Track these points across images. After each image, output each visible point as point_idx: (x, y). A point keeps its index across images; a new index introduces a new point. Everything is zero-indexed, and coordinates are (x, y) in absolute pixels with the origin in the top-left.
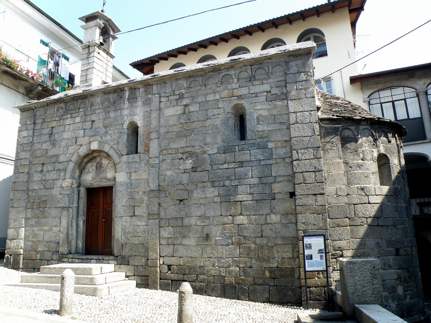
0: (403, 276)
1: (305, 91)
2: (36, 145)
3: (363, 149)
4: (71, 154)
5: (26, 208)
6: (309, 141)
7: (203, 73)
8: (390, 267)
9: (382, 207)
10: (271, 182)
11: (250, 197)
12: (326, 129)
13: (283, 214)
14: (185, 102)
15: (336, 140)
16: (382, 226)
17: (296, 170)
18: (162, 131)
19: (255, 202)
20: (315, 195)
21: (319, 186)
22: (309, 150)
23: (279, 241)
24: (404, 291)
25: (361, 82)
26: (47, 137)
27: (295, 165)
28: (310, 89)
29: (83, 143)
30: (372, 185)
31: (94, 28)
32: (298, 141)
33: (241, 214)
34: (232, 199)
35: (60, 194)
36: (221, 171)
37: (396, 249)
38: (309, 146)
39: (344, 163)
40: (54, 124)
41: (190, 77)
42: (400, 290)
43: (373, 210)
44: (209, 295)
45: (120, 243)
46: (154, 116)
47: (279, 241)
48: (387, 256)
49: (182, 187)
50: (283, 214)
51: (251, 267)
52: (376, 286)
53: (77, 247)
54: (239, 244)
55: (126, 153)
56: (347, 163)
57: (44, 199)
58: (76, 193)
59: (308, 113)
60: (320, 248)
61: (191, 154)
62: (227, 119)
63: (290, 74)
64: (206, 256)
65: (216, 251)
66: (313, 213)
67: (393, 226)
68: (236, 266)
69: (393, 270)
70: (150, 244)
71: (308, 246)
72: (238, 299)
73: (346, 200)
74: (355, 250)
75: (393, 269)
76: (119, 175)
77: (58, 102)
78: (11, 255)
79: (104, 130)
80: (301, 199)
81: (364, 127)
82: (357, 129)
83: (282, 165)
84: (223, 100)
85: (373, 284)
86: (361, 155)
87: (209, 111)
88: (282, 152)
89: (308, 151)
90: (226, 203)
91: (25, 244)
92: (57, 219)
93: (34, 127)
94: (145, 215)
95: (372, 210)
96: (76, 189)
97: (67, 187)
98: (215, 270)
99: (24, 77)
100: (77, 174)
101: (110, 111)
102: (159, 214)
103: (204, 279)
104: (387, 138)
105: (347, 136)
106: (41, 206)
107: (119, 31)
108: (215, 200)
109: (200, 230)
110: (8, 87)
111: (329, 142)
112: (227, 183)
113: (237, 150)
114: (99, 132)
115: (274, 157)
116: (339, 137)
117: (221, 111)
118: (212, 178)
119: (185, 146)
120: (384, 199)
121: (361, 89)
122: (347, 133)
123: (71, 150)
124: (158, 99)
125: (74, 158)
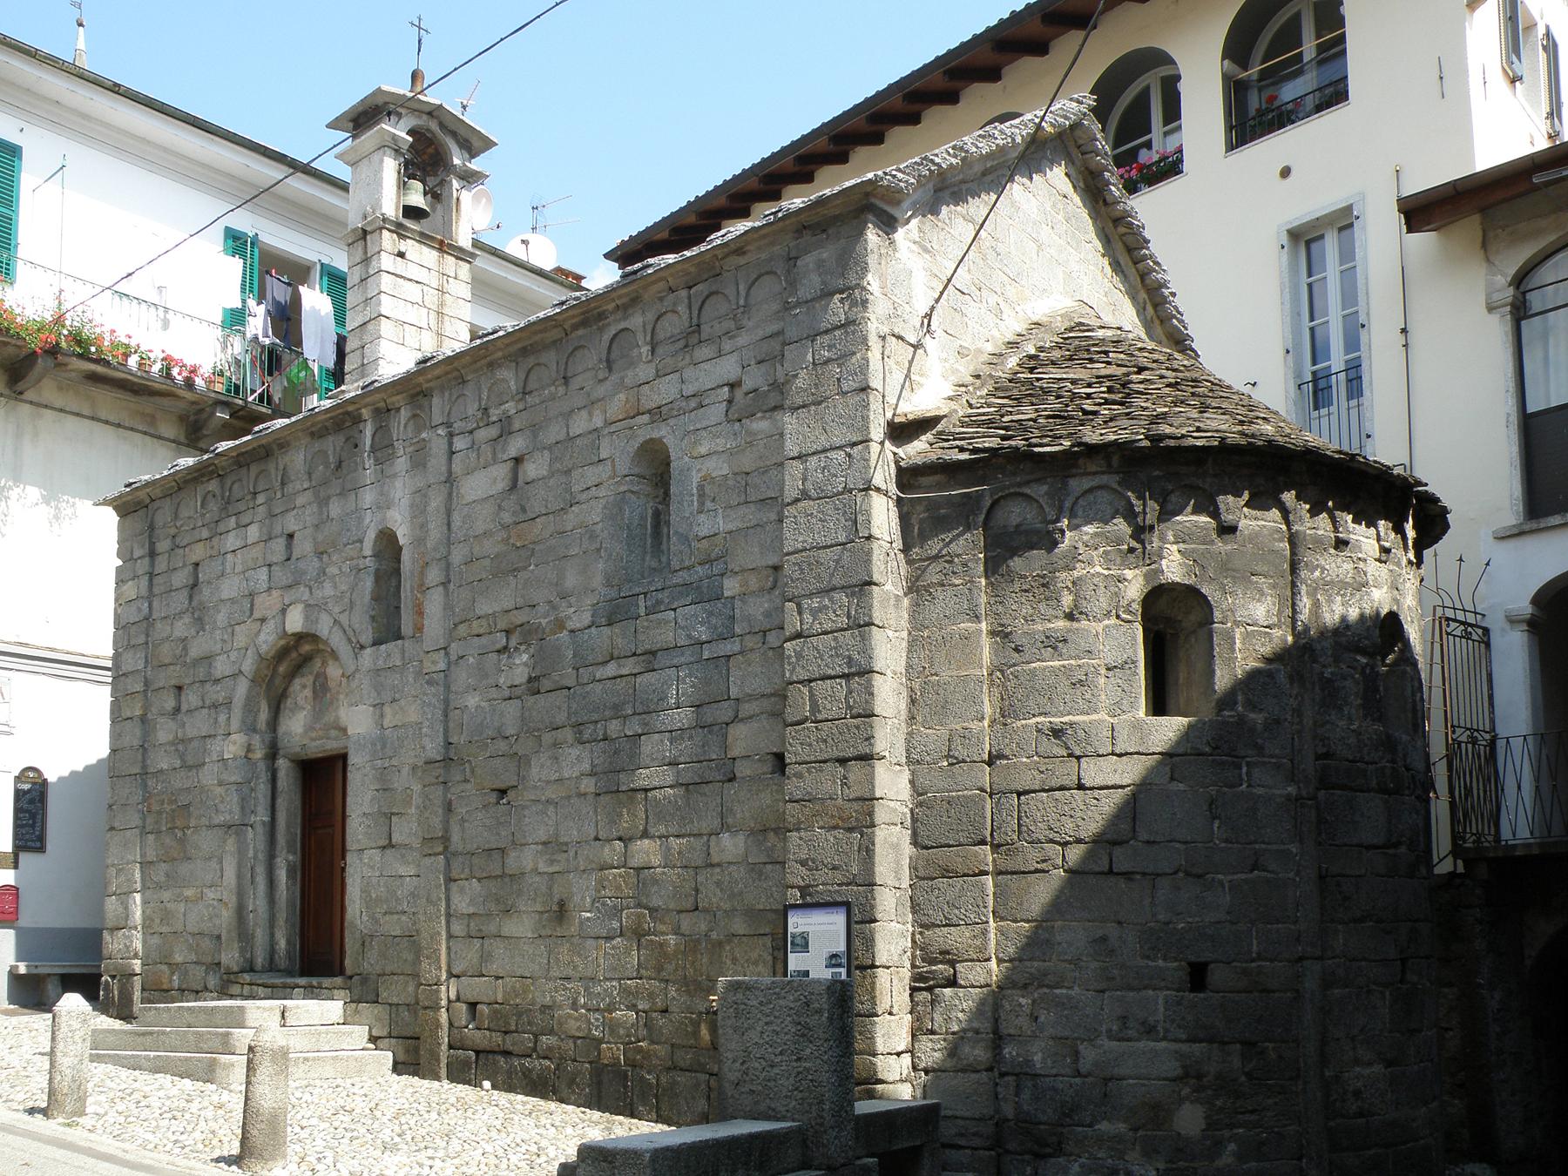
1: (840, 366)
2: (159, 625)
4: (239, 649)
5: (144, 832)
6: (837, 562)
7: (556, 334)
8: (1149, 1031)
10: (726, 719)
11: (669, 776)
12: (932, 505)
13: (752, 832)
14: (516, 446)
15: (968, 546)
16: (1127, 875)
17: (792, 671)
18: (457, 556)
19: (682, 791)
20: (843, 761)
21: (857, 727)
22: (836, 596)
23: (739, 926)
24: (1211, 1125)
25: (1482, 210)
26: (180, 600)
27: (789, 657)
28: (854, 360)
29: (269, 614)
31: (376, 157)
32: (805, 566)
33: (645, 834)
34: (626, 782)
35: (220, 784)
36: (598, 687)
39: (993, 633)
40: (198, 552)
41: (525, 352)
42: (1190, 1120)
44: (562, 1101)
45: (358, 935)
46: (434, 504)
47: (739, 926)
49: (502, 746)
50: (752, 832)
51: (666, 1011)
53: (272, 952)
54: (638, 934)
55: (370, 641)
56: (1007, 635)
57: (183, 800)
58: (264, 777)
59: (840, 456)
60: (834, 950)
61: (521, 633)
62: (621, 500)
63: (798, 304)
64: (557, 974)
65: (580, 955)
66: (835, 827)
67: (1188, 874)
68: (628, 1008)
69: (1164, 1044)
70: (424, 934)
71: (798, 940)
72: (632, 1116)
73: (985, 776)
74: (1010, 961)
75: (1165, 1038)
76: (354, 718)
77: (203, 475)
78: (113, 977)
79: (316, 563)
80: (799, 776)
81: (1087, 483)
83: (755, 657)
84: (613, 428)
85: (799, 1059)
86: (1067, 600)
87: (576, 474)
88: (757, 608)
90: (607, 798)
91: (144, 942)
92: (214, 864)
93: (152, 565)
94: (416, 844)
95: (1093, 815)
96: (262, 766)
97: (234, 759)
98: (576, 1019)
99: (156, 385)
100: (264, 715)
101: (329, 497)
102: (446, 839)
103: (550, 1048)
104: (1215, 514)
105: (1018, 526)
106: (178, 823)
107: (488, 144)
108: (582, 789)
109: (544, 889)
110: (119, 425)
111: (937, 557)
112: (614, 727)
113: (642, 611)
114: (305, 573)
115: (738, 630)
116: (978, 535)
117: (603, 472)
118: (576, 713)
119: (511, 605)
120: (1152, 772)
121: (1484, 245)
122: (1015, 514)
123: (241, 636)
124: (443, 444)
125: (248, 666)
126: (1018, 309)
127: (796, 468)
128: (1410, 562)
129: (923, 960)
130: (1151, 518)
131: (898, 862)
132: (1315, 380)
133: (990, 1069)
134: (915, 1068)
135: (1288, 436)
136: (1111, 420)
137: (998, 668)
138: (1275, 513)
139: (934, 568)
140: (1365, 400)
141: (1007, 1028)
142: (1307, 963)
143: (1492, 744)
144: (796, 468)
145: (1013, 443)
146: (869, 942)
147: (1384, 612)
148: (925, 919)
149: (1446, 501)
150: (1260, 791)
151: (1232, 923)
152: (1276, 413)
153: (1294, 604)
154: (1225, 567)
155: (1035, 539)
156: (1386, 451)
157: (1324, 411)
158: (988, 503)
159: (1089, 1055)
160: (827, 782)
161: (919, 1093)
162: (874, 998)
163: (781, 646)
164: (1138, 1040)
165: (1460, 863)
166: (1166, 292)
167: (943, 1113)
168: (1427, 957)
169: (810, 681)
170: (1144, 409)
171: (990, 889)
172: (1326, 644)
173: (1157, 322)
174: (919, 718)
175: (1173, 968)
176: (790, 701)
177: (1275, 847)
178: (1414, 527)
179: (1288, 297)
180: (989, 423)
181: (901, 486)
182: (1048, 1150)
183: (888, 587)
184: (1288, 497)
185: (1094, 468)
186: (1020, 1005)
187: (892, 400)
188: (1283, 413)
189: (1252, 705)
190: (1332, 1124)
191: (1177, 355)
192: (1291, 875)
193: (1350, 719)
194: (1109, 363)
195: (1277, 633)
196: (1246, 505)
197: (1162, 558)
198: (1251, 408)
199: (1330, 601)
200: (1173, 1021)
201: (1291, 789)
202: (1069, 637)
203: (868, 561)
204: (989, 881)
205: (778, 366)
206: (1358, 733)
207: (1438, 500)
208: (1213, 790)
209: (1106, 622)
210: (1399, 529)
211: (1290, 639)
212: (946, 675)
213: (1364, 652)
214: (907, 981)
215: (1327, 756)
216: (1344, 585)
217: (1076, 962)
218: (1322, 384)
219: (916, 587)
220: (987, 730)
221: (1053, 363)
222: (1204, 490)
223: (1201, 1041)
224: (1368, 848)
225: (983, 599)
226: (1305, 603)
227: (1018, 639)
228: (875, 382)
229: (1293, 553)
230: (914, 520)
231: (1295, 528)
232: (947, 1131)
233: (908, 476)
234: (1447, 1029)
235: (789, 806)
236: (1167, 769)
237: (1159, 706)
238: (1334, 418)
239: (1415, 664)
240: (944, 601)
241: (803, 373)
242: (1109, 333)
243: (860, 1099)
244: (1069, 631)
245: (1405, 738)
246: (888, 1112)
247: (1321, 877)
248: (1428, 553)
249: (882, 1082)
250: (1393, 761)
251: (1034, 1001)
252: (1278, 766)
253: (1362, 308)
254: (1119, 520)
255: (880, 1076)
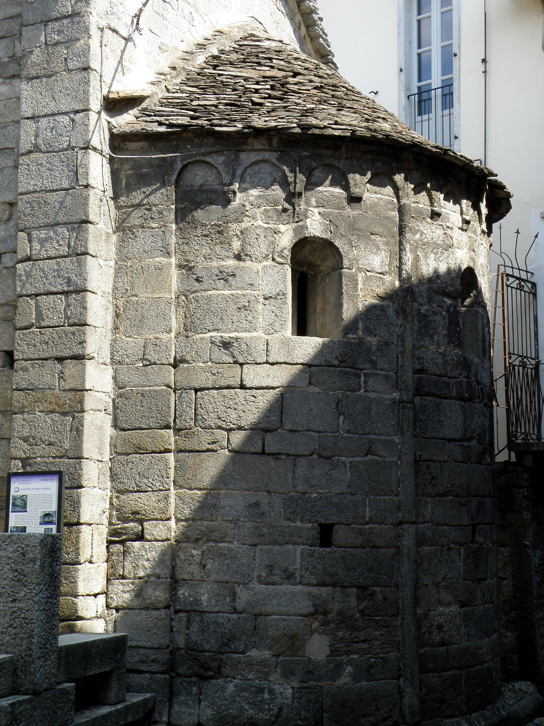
0: (336, 607)
1: (67, 48)
3: (243, 225)
6: (61, 203)
8: (289, 577)
9: (284, 402)
12: (136, 165)
15: (163, 198)
16: (275, 455)
17: (23, 286)
20: (60, 360)
21: (73, 334)
22: (59, 229)
24: (334, 652)
27: (20, 275)
28: (78, 45)
30: (260, 333)
32: (35, 205)
37: (321, 525)
38: (61, 218)
39: (180, 267)
42: (318, 648)
43: (251, 407)
48: (282, 544)
52: (21, 605)
56: (190, 269)
59: (65, 120)
60: (48, 510)
66: (52, 412)
67: (320, 456)
69: (300, 587)
71: (18, 502)
74: (186, 520)
75: (300, 583)
80: (25, 369)
82: (232, 166)
85: (14, 601)
86: (236, 245)
89: (55, 233)
95: (251, 409)
104: (346, 187)
105: (201, 186)
111: (139, 205)
116: (171, 189)
120: (297, 377)
122: (199, 177)
126: (205, 18)
127: (29, 127)
128: (483, 232)
129: (118, 519)
130: (300, 187)
131: (101, 441)
132: (420, 93)
133: (167, 607)
134: (108, 607)
135: (400, 132)
136: (273, 110)
137: (183, 293)
138: (389, 190)
139: (137, 213)
140: (454, 111)
141: (181, 575)
142: (404, 526)
143: (537, 367)
144: (29, 127)
145: (199, 122)
146: (76, 504)
147: (464, 267)
148: (121, 487)
149: (509, 188)
150: (373, 395)
151: (352, 495)
152: (392, 115)
153: (400, 258)
154: (353, 227)
155: (214, 197)
156: (468, 148)
157: (425, 117)
158: (179, 166)
159: (244, 596)
160: (47, 376)
161: (110, 627)
162: (78, 549)
163: (14, 267)
164: (281, 584)
165: (513, 454)
166: (316, 17)
167: (129, 643)
168: (490, 524)
169: (37, 295)
170: (297, 104)
171: (172, 464)
172: (423, 288)
173: (308, 39)
174: (122, 329)
175: (307, 528)
176: (20, 310)
177: (383, 438)
178: (487, 206)
179: (403, 29)
180: (182, 106)
181: (113, 148)
182: (210, 673)
183: (101, 226)
184: (399, 178)
185: (259, 147)
186: (192, 556)
187: (107, 79)
188: (396, 115)
189: (369, 331)
190: (422, 651)
191: (322, 66)
192: (395, 459)
193: (438, 344)
194: (272, 67)
195: (388, 278)
196: (369, 182)
197: (307, 217)
198: (374, 110)
199: (426, 257)
200: (307, 569)
201: (396, 395)
202: (237, 272)
203: (86, 205)
204: (171, 457)
205: (17, 43)
206: (443, 355)
207: (503, 187)
208: (339, 393)
209: (265, 263)
210: (476, 207)
211: (397, 283)
212: (143, 296)
213: (449, 295)
214: (105, 536)
215: (421, 371)
216: (436, 246)
217: (235, 522)
218: (425, 96)
219: (121, 227)
220: (174, 341)
221: (231, 63)
222: (339, 169)
223: (327, 585)
224: (450, 440)
225: (173, 240)
226: (408, 257)
227: (199, 272)
228: (94, 64)
229: (401, 220)
230: (123, 175)
231: (403, 201)
232: (132, 659)
233: (119, 141)
234: (503, 579)
235: (16, 393)
236: (307, 376)
237: (302, 328)
238: (432, 123)
239: (484, 306)
240: (144, 240)
241: (37, 51)
242: (273, 44)
243: (63, 633)
244: (237, 268)
245: (476, 360)
246: (86, 644)
247: (416, 462)
248: (495, 226)
249: (81, 618)
250: (468, 377)
251: (203, 552)
252: (387, 377)
253: (455, 41)
254: (276, 187)
255: (80, 614)
